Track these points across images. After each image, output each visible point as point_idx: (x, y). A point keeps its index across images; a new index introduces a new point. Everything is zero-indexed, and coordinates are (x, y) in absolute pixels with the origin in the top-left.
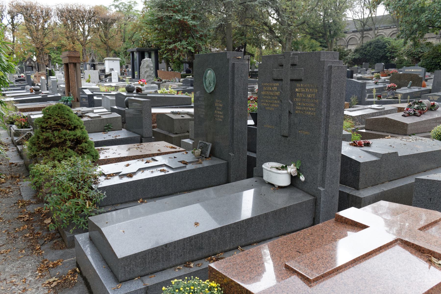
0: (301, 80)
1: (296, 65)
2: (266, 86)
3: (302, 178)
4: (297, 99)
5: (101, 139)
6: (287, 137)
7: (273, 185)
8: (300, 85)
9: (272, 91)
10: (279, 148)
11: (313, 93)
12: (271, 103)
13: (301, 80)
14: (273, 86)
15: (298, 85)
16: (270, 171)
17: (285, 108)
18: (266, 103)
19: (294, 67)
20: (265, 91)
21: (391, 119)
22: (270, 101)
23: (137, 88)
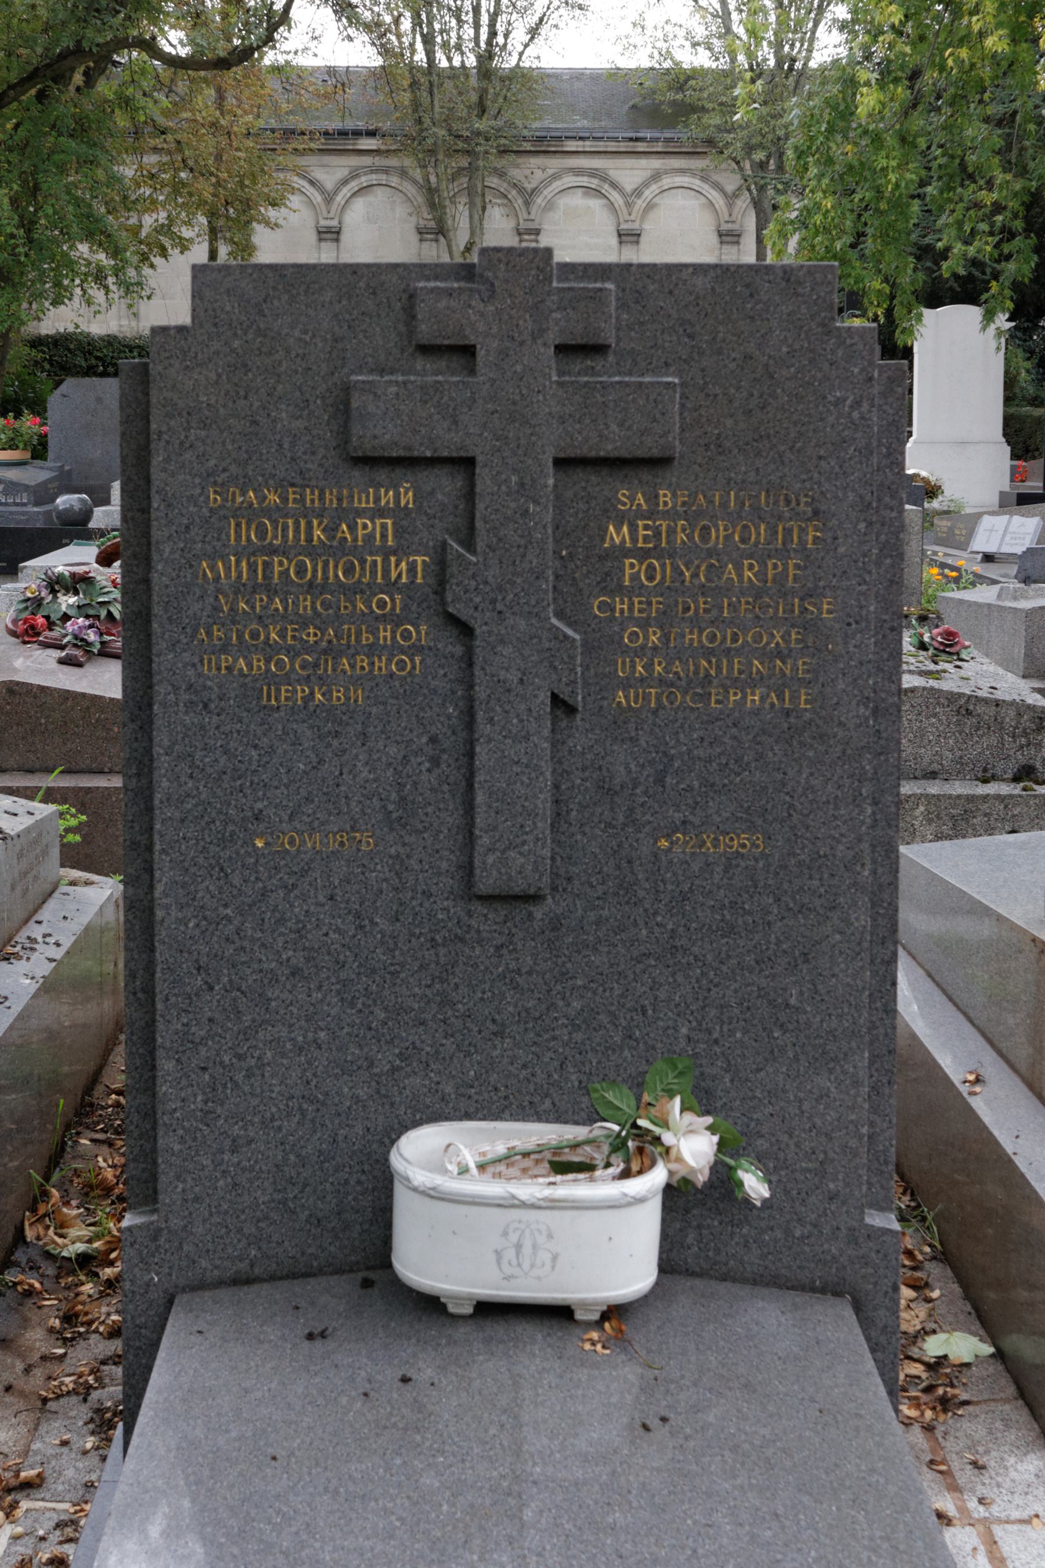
0: (659, 463)
1: (598, 349)
2: (250, 513)
3: (754, 1184)
4: (621, 605)
5: (141, 1435)
6: (534, 898)
7: (559, 1314)
8: (653, 498)
9: (338, 550)
10: (446, 1002)
11: (784, 553)
12: (331, 651)
13: (659, 463)
14: (348, 514)
15: (629, 496)
16: (553, 1205)
17: (513, 677)
18: (269, 650)
19: (578, 364)
20: (250, 552)
21: (43, 689)
22: (311, 635)
23: (17, 581)
